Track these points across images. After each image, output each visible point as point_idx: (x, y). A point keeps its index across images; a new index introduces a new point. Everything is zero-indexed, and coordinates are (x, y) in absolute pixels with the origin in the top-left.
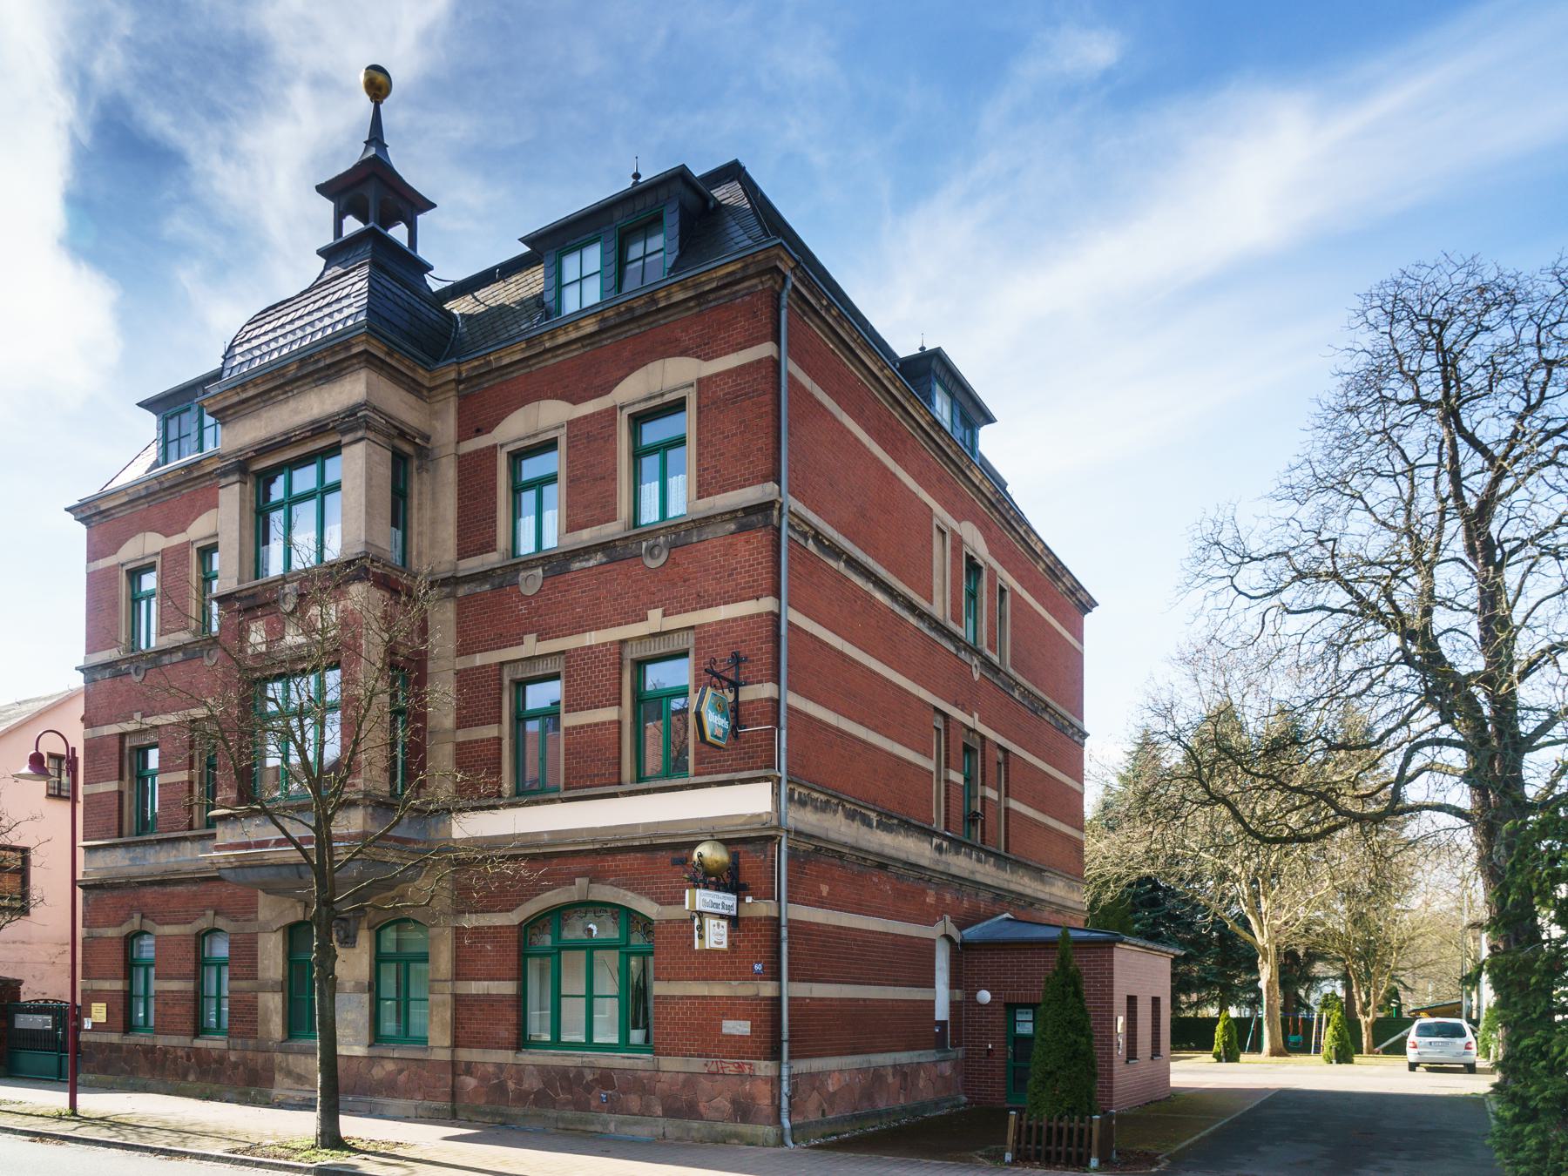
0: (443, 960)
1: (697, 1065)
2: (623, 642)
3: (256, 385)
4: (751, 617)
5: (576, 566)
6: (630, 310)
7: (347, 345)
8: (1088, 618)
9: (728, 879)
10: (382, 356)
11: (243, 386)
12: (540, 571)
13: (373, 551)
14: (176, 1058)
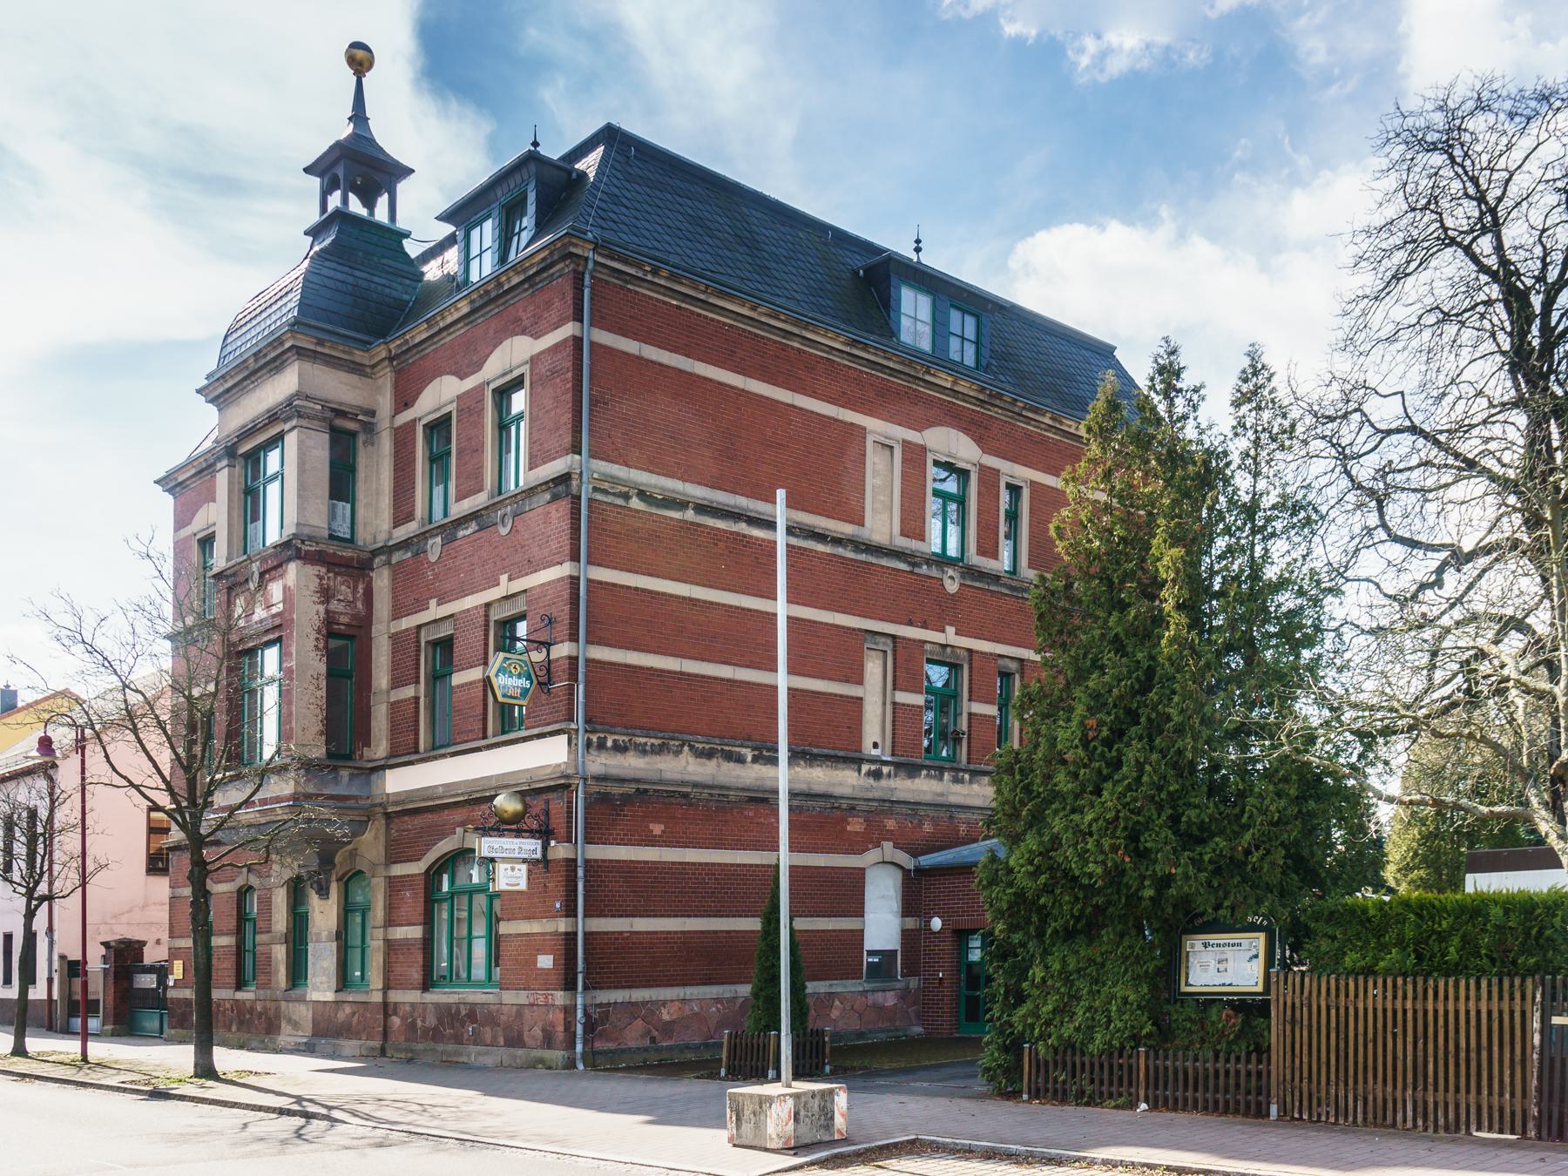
0: (378, 913)
1: (522, 998)
2: (488, 605)
5: (461, 533)
6: (487, 292)
7: (279, 341)
10: (312, 347)
12: (438, 540)
13: (306, 531)
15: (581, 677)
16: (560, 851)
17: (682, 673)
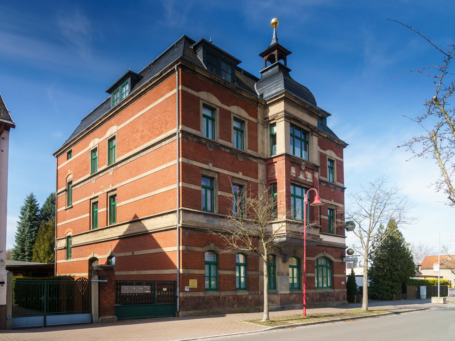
3: (299, 102)
14: (229, 300)
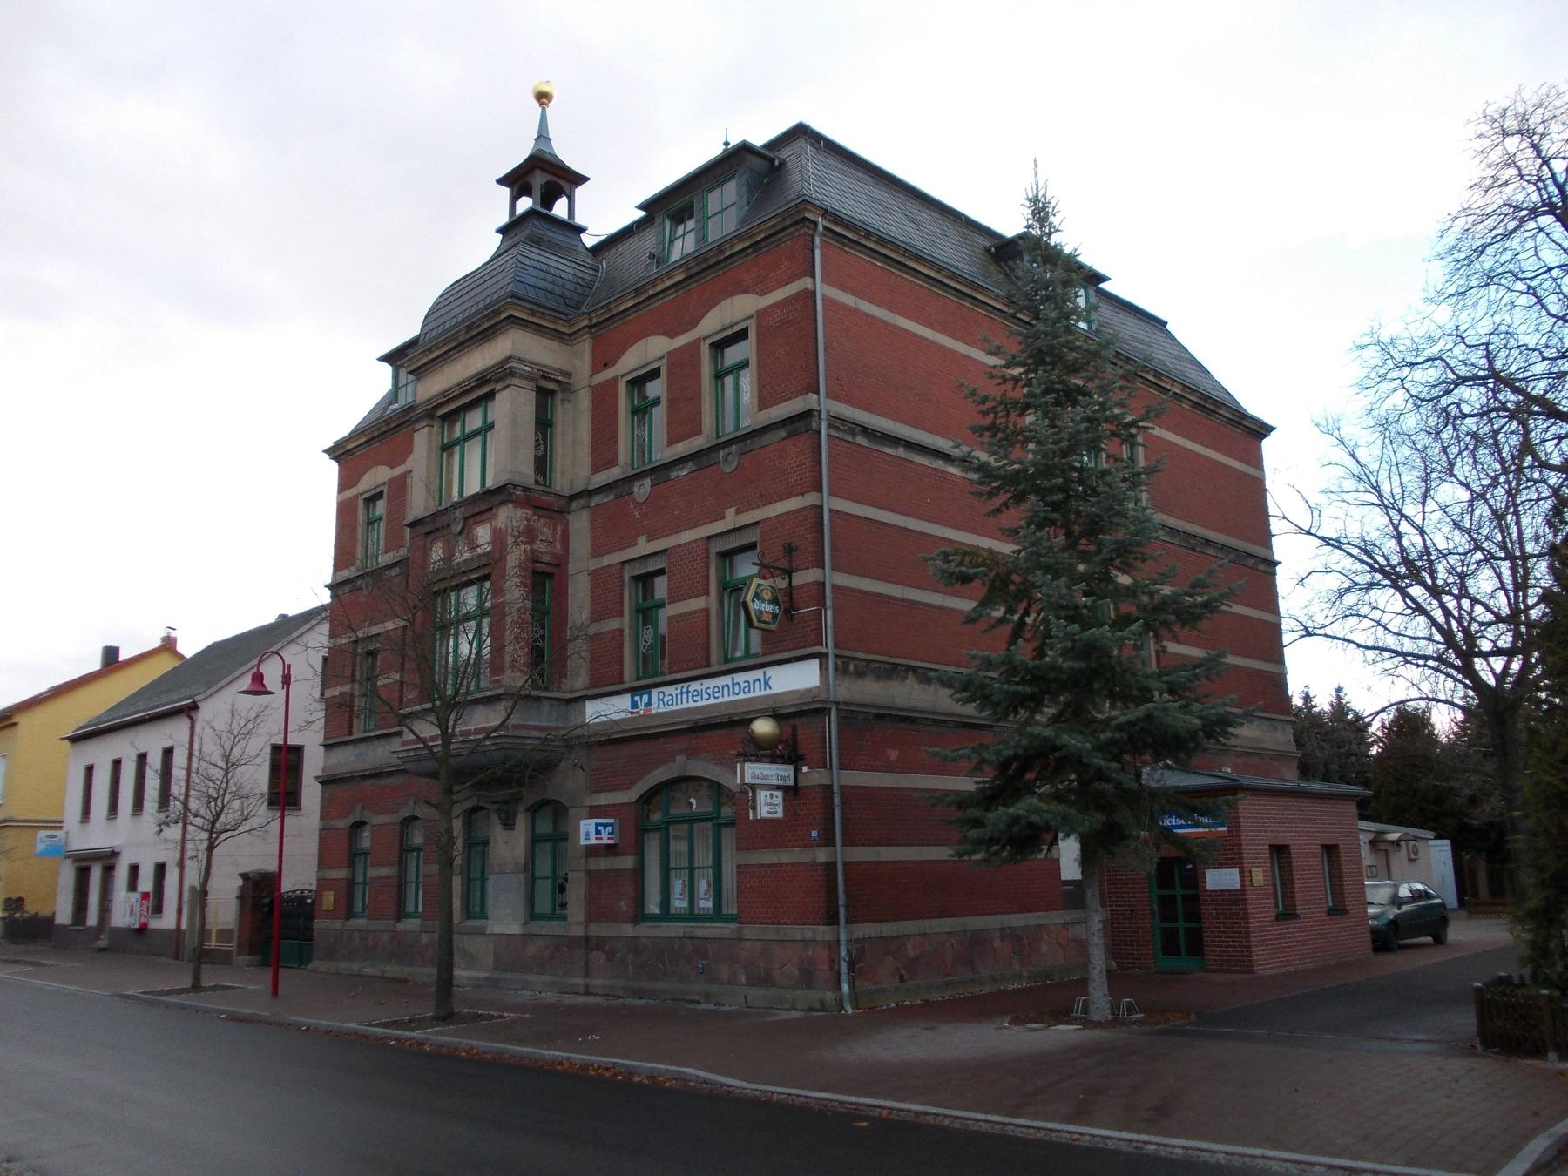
4: (798, 510)
5: (674, 474)
8: (1266, 443)
9: (785, 750)
11: (430, 350)
15: (829, 602)
16: (812, 776)
17: (903, 600)
